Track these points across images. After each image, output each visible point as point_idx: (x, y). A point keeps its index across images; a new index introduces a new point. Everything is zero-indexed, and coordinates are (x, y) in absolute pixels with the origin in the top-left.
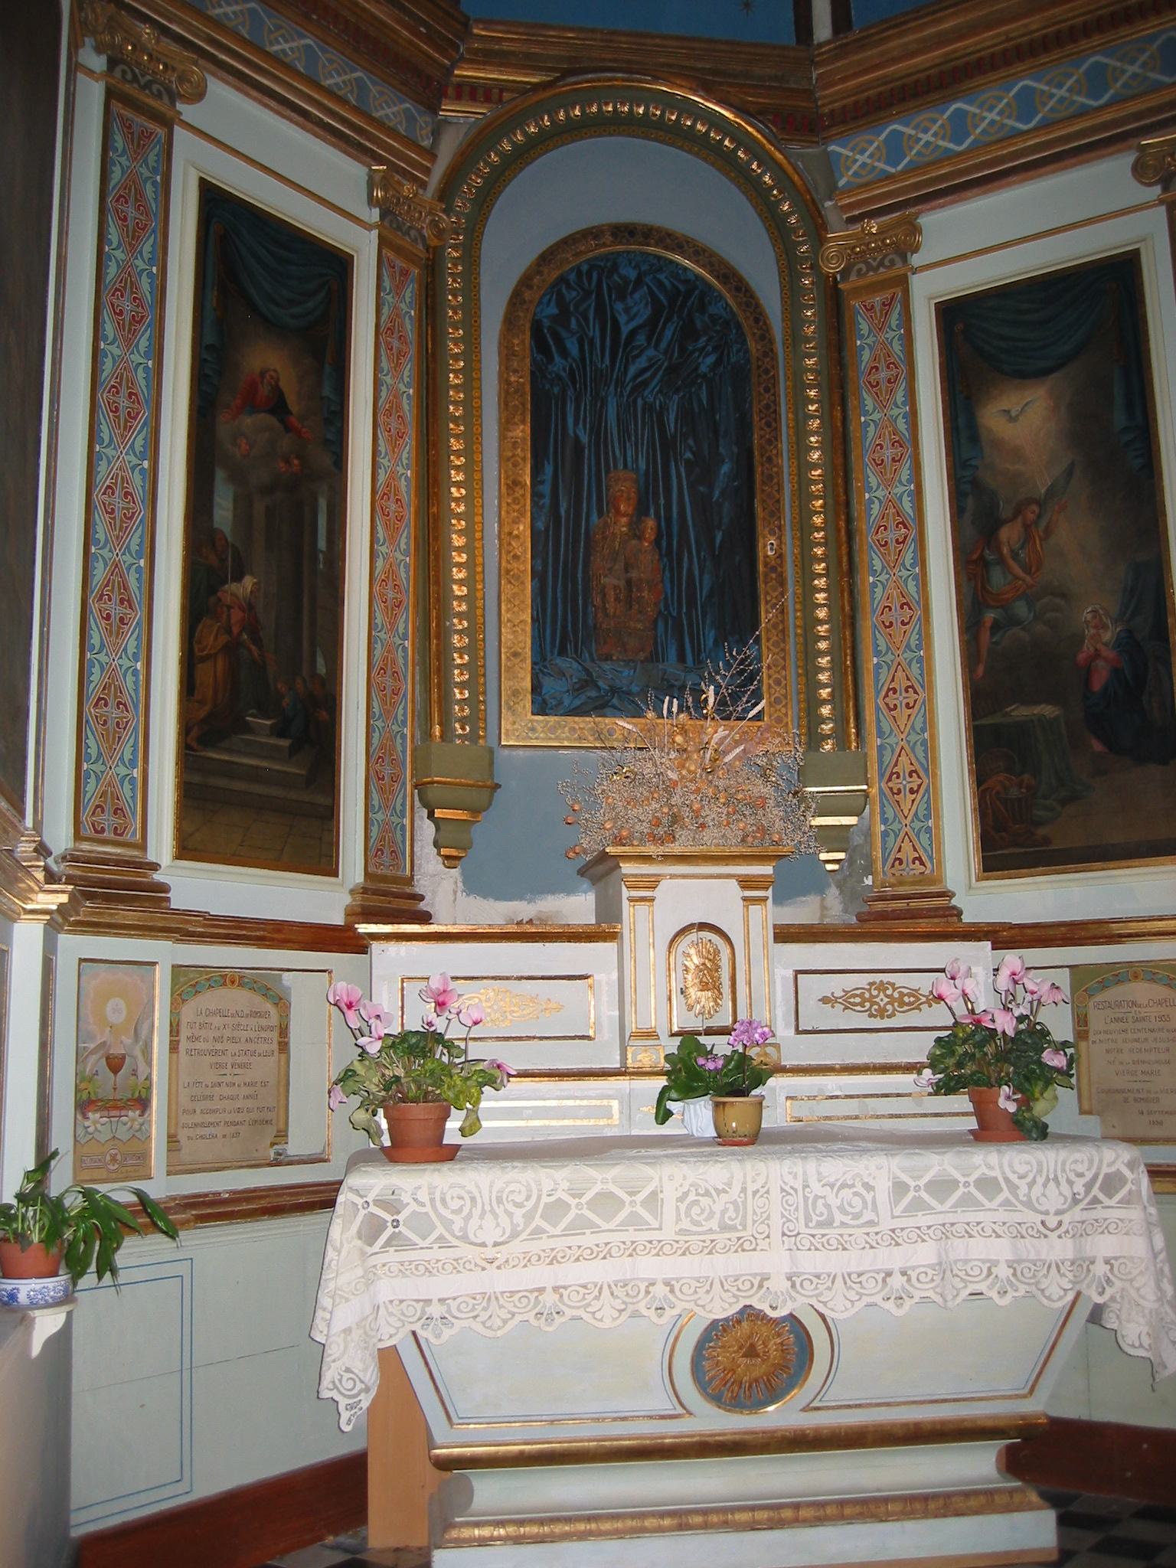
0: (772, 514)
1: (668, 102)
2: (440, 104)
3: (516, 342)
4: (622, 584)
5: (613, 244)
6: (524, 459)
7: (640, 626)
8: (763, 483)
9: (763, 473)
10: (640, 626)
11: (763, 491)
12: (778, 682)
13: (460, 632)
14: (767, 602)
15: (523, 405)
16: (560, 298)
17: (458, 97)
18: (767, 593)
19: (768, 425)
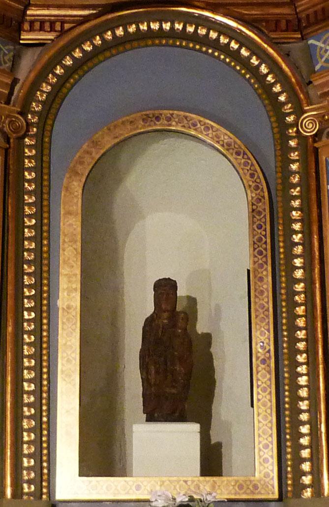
1: (188, 19)
2: (20, 35)
5: (144, 127)
7: (174, 391)
13: (29, 274)
17: (32, 29)
18: (258, 380)
19: (259, 213)
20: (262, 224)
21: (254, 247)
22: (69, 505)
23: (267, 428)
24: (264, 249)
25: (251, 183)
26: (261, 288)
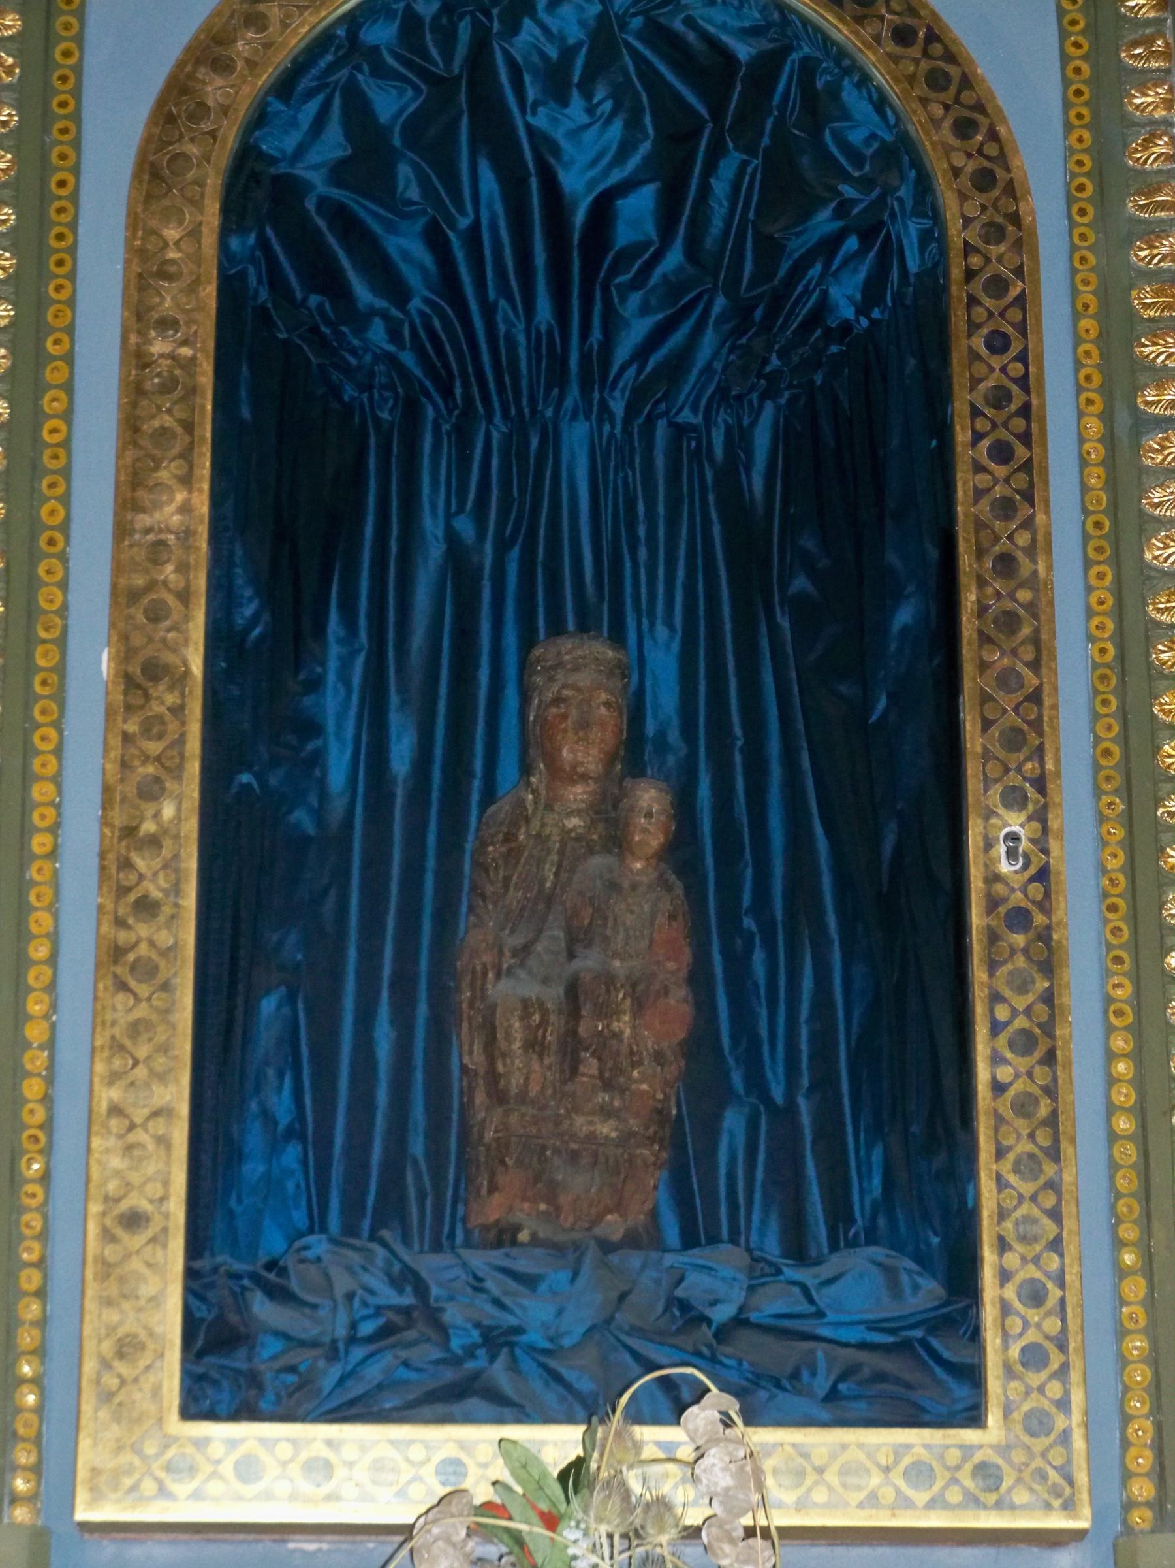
0: (1014, 740)
3: (172, 233)
4: (554, 994)
6: (184, 596)
7: (607, 1129)
8: (985, 639)
9: (982, 610)
10: (607, 1129)
11: (983, 666)
12: (1035, 1296)
14: (996, 1028)
15: (189, 427)
16: (358, 110)
18: (996, 998)
19: (1002, 453)
20: (1009, 330)
21: (974, 431)
22: (138, 1551)
23: (1036, 1212)
24: (1018, 436)
25: (959, 160)
26: (1010, 605)
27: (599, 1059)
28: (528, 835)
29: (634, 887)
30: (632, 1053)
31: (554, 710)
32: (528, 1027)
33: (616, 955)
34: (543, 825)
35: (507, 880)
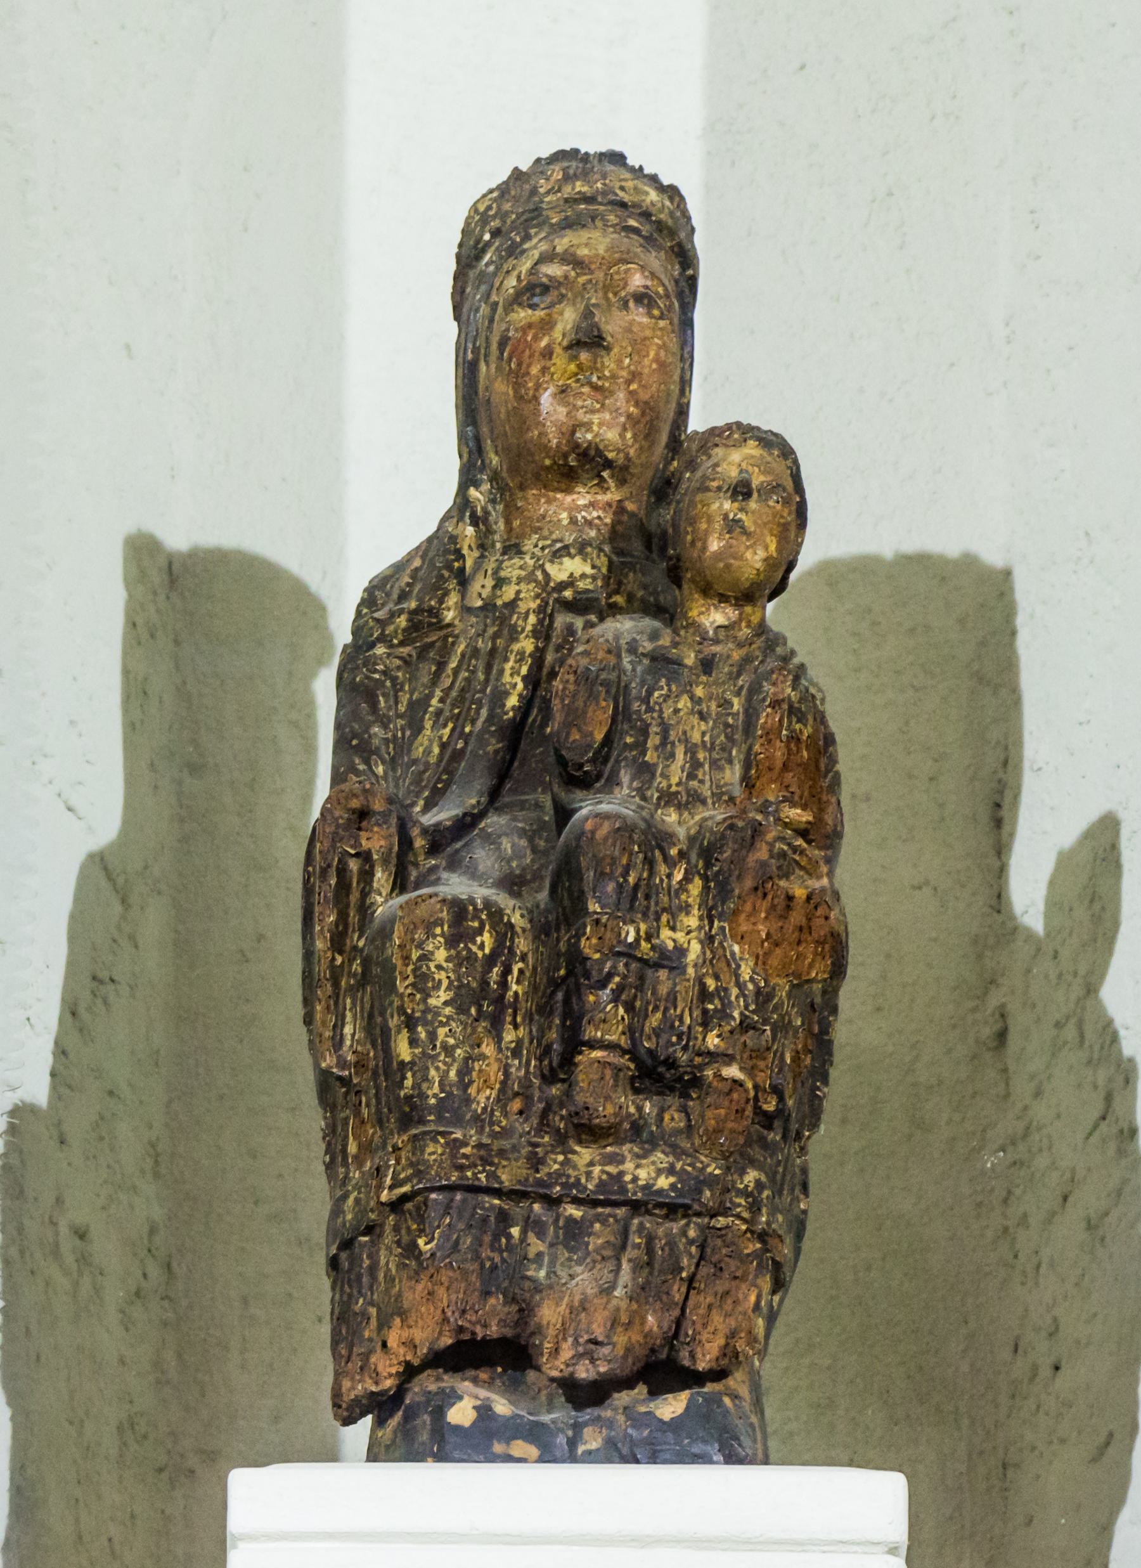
27: (630, 1007)
28: (465, 610)
29: (707, 665)
30: (704, 995)
31: (522, 315)
32: (463, 961)
33: (668, 798)
34: (500, 583)
35: (418, 707)
